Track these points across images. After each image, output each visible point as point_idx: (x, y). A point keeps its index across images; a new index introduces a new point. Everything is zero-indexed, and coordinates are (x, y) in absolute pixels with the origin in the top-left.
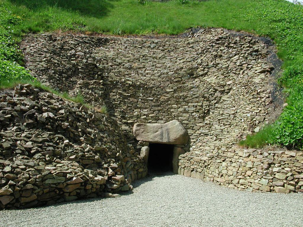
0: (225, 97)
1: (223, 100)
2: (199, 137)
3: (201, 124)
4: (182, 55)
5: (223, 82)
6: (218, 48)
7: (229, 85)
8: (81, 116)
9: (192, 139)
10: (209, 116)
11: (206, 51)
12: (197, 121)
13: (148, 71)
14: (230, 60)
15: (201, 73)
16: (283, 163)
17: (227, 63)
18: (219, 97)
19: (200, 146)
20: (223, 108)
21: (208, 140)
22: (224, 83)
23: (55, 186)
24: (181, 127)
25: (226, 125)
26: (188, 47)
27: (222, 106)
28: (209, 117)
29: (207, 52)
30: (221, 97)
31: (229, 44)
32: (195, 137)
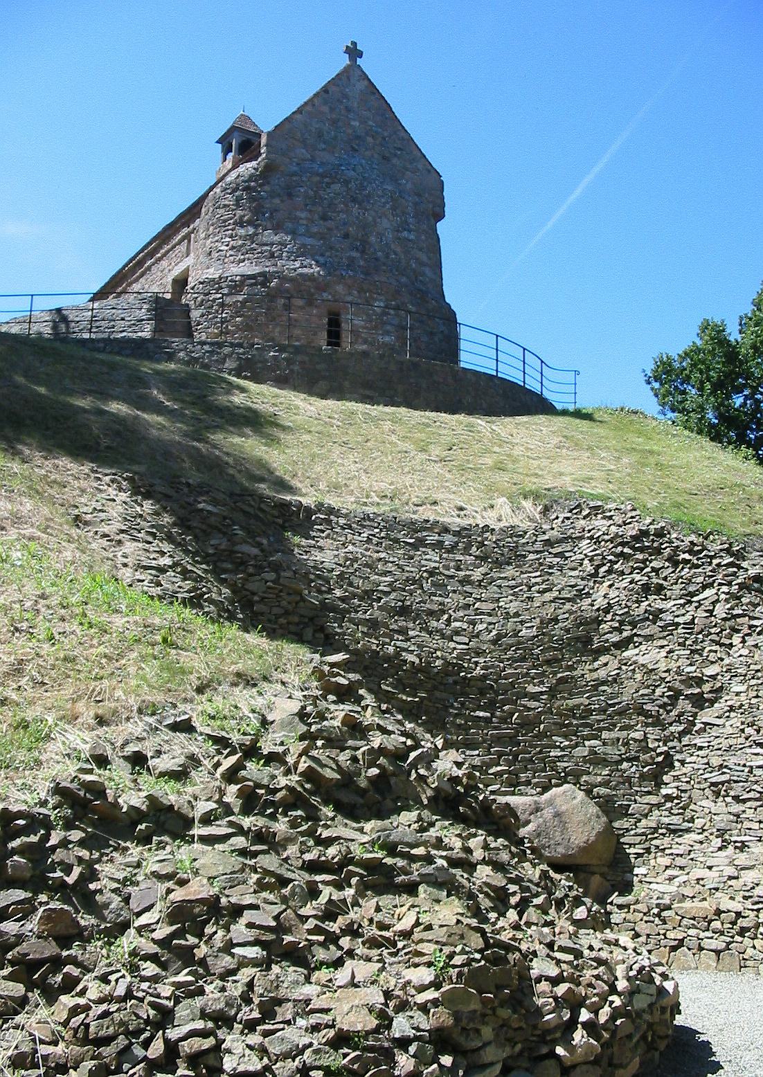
0: (707, 716)
1: (706, 724)
2: (652, 839)
3: (653, 799)
4: (540, 576)
5: (693, 669)
6: (644, 561)
7: (714, 677)
9: (627, 846)
10: (671, 773)
11: (605, 568)
12: (638, 789)
13: (458, 624)
14: (692, 602)
15: (615, 638)
17: (688, 612)
18: (690, 714)
19: (667, 867)
20: (715, 747)
21: (690, 848)
22: (695, 671)
24: (593, 809)
25: (744, 801)
26: (550, 553)
27: (709, 742)
28: (674, 776)
29: (609, 572)
30: (695, 715)
32: (639, 838)
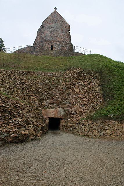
8: (17, 106)
15: (72, 87)
16: (109, 126)
23: (3, 138)
31: (84, 74)
